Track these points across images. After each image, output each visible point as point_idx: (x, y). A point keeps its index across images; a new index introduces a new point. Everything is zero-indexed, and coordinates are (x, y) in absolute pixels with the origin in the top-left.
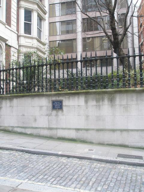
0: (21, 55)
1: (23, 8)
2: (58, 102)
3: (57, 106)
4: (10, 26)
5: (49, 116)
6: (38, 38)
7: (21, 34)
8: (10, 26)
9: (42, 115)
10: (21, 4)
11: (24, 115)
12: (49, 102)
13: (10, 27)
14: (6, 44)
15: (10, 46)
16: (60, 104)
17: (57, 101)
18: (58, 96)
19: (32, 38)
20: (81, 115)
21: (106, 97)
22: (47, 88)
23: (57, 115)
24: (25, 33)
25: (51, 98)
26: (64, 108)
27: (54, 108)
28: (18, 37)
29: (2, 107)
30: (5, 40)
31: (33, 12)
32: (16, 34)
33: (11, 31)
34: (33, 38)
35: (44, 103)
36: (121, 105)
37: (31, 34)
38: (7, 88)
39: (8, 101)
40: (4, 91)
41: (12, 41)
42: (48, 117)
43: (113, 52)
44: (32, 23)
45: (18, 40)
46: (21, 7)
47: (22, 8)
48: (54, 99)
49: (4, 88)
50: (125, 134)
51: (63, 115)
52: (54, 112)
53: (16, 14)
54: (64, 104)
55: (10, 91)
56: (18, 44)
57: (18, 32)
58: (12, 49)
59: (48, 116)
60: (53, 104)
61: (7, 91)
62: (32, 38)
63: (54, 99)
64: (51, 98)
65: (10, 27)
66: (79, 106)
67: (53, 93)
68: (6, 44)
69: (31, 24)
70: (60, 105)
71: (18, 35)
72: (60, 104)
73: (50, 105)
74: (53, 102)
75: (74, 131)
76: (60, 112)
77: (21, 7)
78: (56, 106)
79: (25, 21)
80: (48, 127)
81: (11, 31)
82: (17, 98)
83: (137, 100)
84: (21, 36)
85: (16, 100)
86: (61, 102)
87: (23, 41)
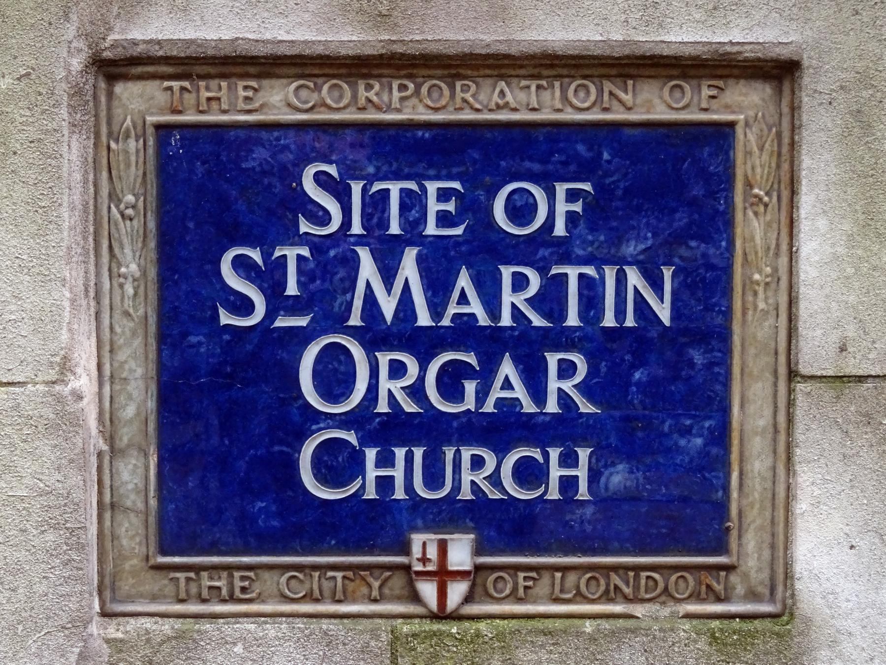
2: (480, 154)
16: (637, 293)
72: (637, 293)
78: (389, 382)
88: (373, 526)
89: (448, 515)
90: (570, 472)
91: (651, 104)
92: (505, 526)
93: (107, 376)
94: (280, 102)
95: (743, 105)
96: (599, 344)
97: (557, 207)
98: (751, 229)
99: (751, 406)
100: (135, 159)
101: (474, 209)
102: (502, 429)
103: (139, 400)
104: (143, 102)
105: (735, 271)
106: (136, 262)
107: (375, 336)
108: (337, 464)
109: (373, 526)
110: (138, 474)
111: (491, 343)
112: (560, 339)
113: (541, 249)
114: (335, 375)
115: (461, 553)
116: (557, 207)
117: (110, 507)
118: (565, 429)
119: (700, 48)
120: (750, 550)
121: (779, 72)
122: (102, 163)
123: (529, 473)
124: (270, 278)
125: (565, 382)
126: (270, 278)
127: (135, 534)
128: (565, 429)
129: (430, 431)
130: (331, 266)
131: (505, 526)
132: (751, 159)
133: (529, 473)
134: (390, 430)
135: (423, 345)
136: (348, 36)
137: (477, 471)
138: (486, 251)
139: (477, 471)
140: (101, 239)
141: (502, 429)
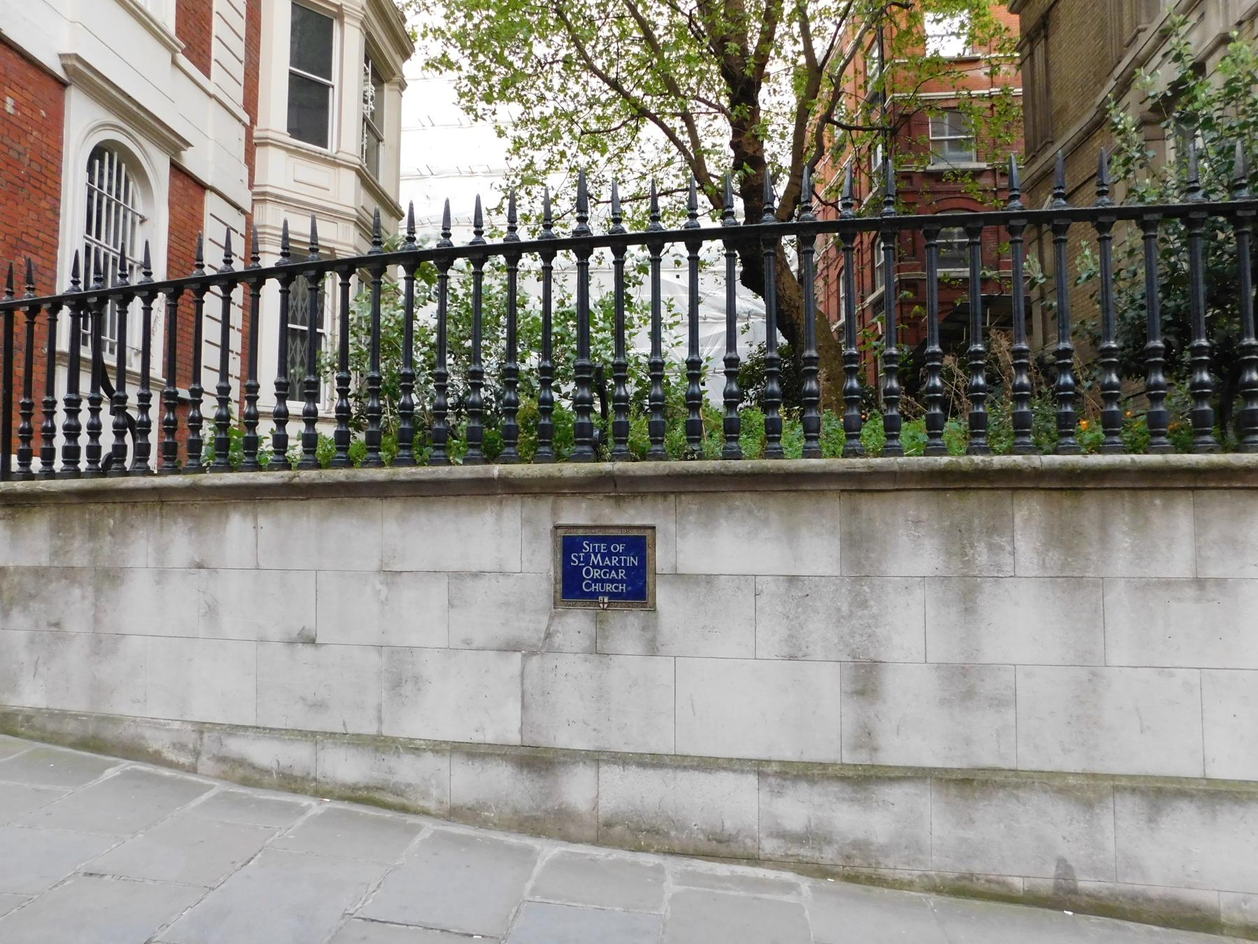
2: (609, 540)
3: (605, 576)
4: (206, 71)
5: (534, 653)
6: (365, 165)
7: (270, 134)
8: (206, 71)
12: (536, 536)
13: (208, 77)
14: (177, 169)
15: (202, 187)
16: (632, 561)
17: (607, 539)
18: (501, 503)
20: (805, 658)
21: (1027, 517)
23: (597, 650)
24: (294, 131)
25: (555, 512)
26: (663, 595)
27: (572, 587)
28: (251, 147)
30: (173, 143)
32: (239, 126)
34: (340, 165)
35: (503, 548)
37: (326, 147)
38: (169, 428)
39: (700, 306)
40: (147, 447)
41: (212, 158)
43: (738, 284)
44: (335, 81)
45: (250, 159)
48: (577, 514)
49: (148, 424)
50: (1184, 816)
51: (652, 648)
53: (240, 76)
54: (662, 558)
56: (251, 186)
57: (254, 121)
58: (210, 201)
59: (517, 657)
61: (168, 451)
62: (334, 163)
63: (577, 514)
64: (555, 512)
65: (208, 77)
66: (792, 579)
67: (570, 469)
68: (177, 169)
69: (326, 87)
71: (249, 131)
72: (632, 561)
73: (541, 565)
74: (570, 545)
75: (752, 779)
76: (626, 626)
78: (596, 574)
79: (292, 64)
80: (515, 738)
82: (501, 503)
84: (266, 144)
85: (249, 523)
86: (637, 545)
87: (282, 169)
88: (594, 595)
89: (605, 594)
90: (622, 588)
91: (635, 533)
92: (612, 595)
93: (555, 572)
94: (581, 533)
95: (648, 533)
96: (626, 568)
97: (620, 548)
98: (649, 551)
99: (649, 578)
100: (560, 540)
101: (608, 548)
102: (612, 581)
103: (560, 576)
104: (561, 532)
105: (60, 489)
106: (559, 556)
107: (594, 567)
108: (588, 586)
109: (594, 595)
110: (560, 587)
111: (611, 568)
112: (621, 567)
113: (618, 554)
114: (588, 572)
115: (606, 600)
116: (620, 548)
117: (555, 592)
118: (622, 581)
119: (651, 587)
120: (650, 600)
121: (653, 528)
122: (555, 541)
123: (617, 588)
124: (579, 558)
125: (622, 574)
126: (579, 558)
127: (559, 596)
128: (622, 581)
129: (602, 581)
130: (587, 557)
131: (612, 595)
132: (649, 541)
133: (617, 588)
134: (595, 581)
135: (601, 568)
136: (590, 523)
137: (609, 587)
138: (610, 554)
139: (609, 587)
140: (555, 553)
141: (612, 581)
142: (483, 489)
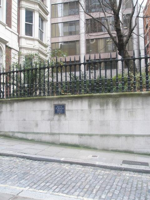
0: (22, 57)
1: (24, 8)
2: (61, 106)
3: (60, 110)
4: (10, 27)
5: (51, 121)
6: (39, 39)
7: (22, 36)
8: (10, 27)
9: (44, 119)
10: (22, 4)
11: (25, 120)
12: (51, 107)
13: (11, 28)
14: (6, 46)
15: (11, 48)
16: (63, 108)
17: (60, 105)
18: (61, 100)
19: (33, 40)
20: (84, 120)
21: (111, 101)
22: (49, 92)
23: (59, 120)
24: (26, 34)
25: (54, 102)
26: (67, 113)
27: (56, 112)
28: (19, 38)
29: (2, 112)
30: (5, 42)
31: (34, 12)
32: (16, 36)
33: (12, 32)
34: (35, 40)
35: (46, 107)
36: (126, 110)
37: (32, 36)
38: (7, 92)
40: (4, 95)
41: (13, 43)
42: (51, 121)
43: (118, 54)
44: (33, 24)
45: (19, 42)
46: (22, 7)
47: (23, 8)
48: (56, 103)
49: (4, 92)
50: (130, 139)
51: (66, 120)
52: (57, 117)
54: (67, 108)
55: (10, 95)
56: (19, 45)
57: (19, 34)
58: (13, 51)
59: (50, 121)
60: (55, 109)
61: (7, 95)
62: (33, 40)
63: (56, 103)
64: (54, 102)
65: (11, 28)
66: (82, 110)
67: (55, 96)
68: (6, 46)
69: (32, 25)
70: (63, 110)
71: (18, 36)
72: (63, 108)
73: (53, 109)
74: (56, 106)
75: (78, 136)
76: (63, 116)
77: (22, 7)
78: (59, 110)
79: (26, 22)
80: (50, 132)
81: (12, 32)
82: (18, 102)
83: (143, 104)
85: (17, 104)
86: (64, 106)
87: (24, 43)
142: (29, 100)
